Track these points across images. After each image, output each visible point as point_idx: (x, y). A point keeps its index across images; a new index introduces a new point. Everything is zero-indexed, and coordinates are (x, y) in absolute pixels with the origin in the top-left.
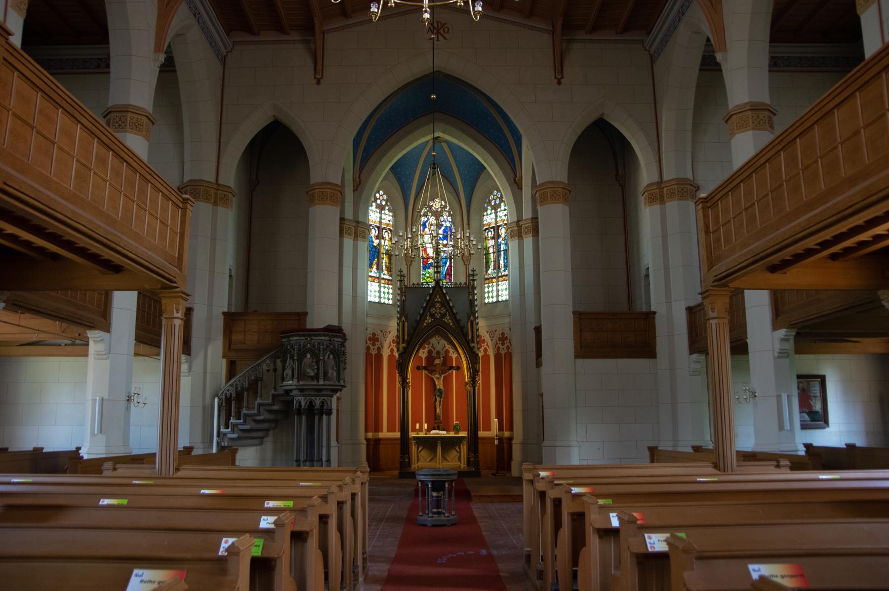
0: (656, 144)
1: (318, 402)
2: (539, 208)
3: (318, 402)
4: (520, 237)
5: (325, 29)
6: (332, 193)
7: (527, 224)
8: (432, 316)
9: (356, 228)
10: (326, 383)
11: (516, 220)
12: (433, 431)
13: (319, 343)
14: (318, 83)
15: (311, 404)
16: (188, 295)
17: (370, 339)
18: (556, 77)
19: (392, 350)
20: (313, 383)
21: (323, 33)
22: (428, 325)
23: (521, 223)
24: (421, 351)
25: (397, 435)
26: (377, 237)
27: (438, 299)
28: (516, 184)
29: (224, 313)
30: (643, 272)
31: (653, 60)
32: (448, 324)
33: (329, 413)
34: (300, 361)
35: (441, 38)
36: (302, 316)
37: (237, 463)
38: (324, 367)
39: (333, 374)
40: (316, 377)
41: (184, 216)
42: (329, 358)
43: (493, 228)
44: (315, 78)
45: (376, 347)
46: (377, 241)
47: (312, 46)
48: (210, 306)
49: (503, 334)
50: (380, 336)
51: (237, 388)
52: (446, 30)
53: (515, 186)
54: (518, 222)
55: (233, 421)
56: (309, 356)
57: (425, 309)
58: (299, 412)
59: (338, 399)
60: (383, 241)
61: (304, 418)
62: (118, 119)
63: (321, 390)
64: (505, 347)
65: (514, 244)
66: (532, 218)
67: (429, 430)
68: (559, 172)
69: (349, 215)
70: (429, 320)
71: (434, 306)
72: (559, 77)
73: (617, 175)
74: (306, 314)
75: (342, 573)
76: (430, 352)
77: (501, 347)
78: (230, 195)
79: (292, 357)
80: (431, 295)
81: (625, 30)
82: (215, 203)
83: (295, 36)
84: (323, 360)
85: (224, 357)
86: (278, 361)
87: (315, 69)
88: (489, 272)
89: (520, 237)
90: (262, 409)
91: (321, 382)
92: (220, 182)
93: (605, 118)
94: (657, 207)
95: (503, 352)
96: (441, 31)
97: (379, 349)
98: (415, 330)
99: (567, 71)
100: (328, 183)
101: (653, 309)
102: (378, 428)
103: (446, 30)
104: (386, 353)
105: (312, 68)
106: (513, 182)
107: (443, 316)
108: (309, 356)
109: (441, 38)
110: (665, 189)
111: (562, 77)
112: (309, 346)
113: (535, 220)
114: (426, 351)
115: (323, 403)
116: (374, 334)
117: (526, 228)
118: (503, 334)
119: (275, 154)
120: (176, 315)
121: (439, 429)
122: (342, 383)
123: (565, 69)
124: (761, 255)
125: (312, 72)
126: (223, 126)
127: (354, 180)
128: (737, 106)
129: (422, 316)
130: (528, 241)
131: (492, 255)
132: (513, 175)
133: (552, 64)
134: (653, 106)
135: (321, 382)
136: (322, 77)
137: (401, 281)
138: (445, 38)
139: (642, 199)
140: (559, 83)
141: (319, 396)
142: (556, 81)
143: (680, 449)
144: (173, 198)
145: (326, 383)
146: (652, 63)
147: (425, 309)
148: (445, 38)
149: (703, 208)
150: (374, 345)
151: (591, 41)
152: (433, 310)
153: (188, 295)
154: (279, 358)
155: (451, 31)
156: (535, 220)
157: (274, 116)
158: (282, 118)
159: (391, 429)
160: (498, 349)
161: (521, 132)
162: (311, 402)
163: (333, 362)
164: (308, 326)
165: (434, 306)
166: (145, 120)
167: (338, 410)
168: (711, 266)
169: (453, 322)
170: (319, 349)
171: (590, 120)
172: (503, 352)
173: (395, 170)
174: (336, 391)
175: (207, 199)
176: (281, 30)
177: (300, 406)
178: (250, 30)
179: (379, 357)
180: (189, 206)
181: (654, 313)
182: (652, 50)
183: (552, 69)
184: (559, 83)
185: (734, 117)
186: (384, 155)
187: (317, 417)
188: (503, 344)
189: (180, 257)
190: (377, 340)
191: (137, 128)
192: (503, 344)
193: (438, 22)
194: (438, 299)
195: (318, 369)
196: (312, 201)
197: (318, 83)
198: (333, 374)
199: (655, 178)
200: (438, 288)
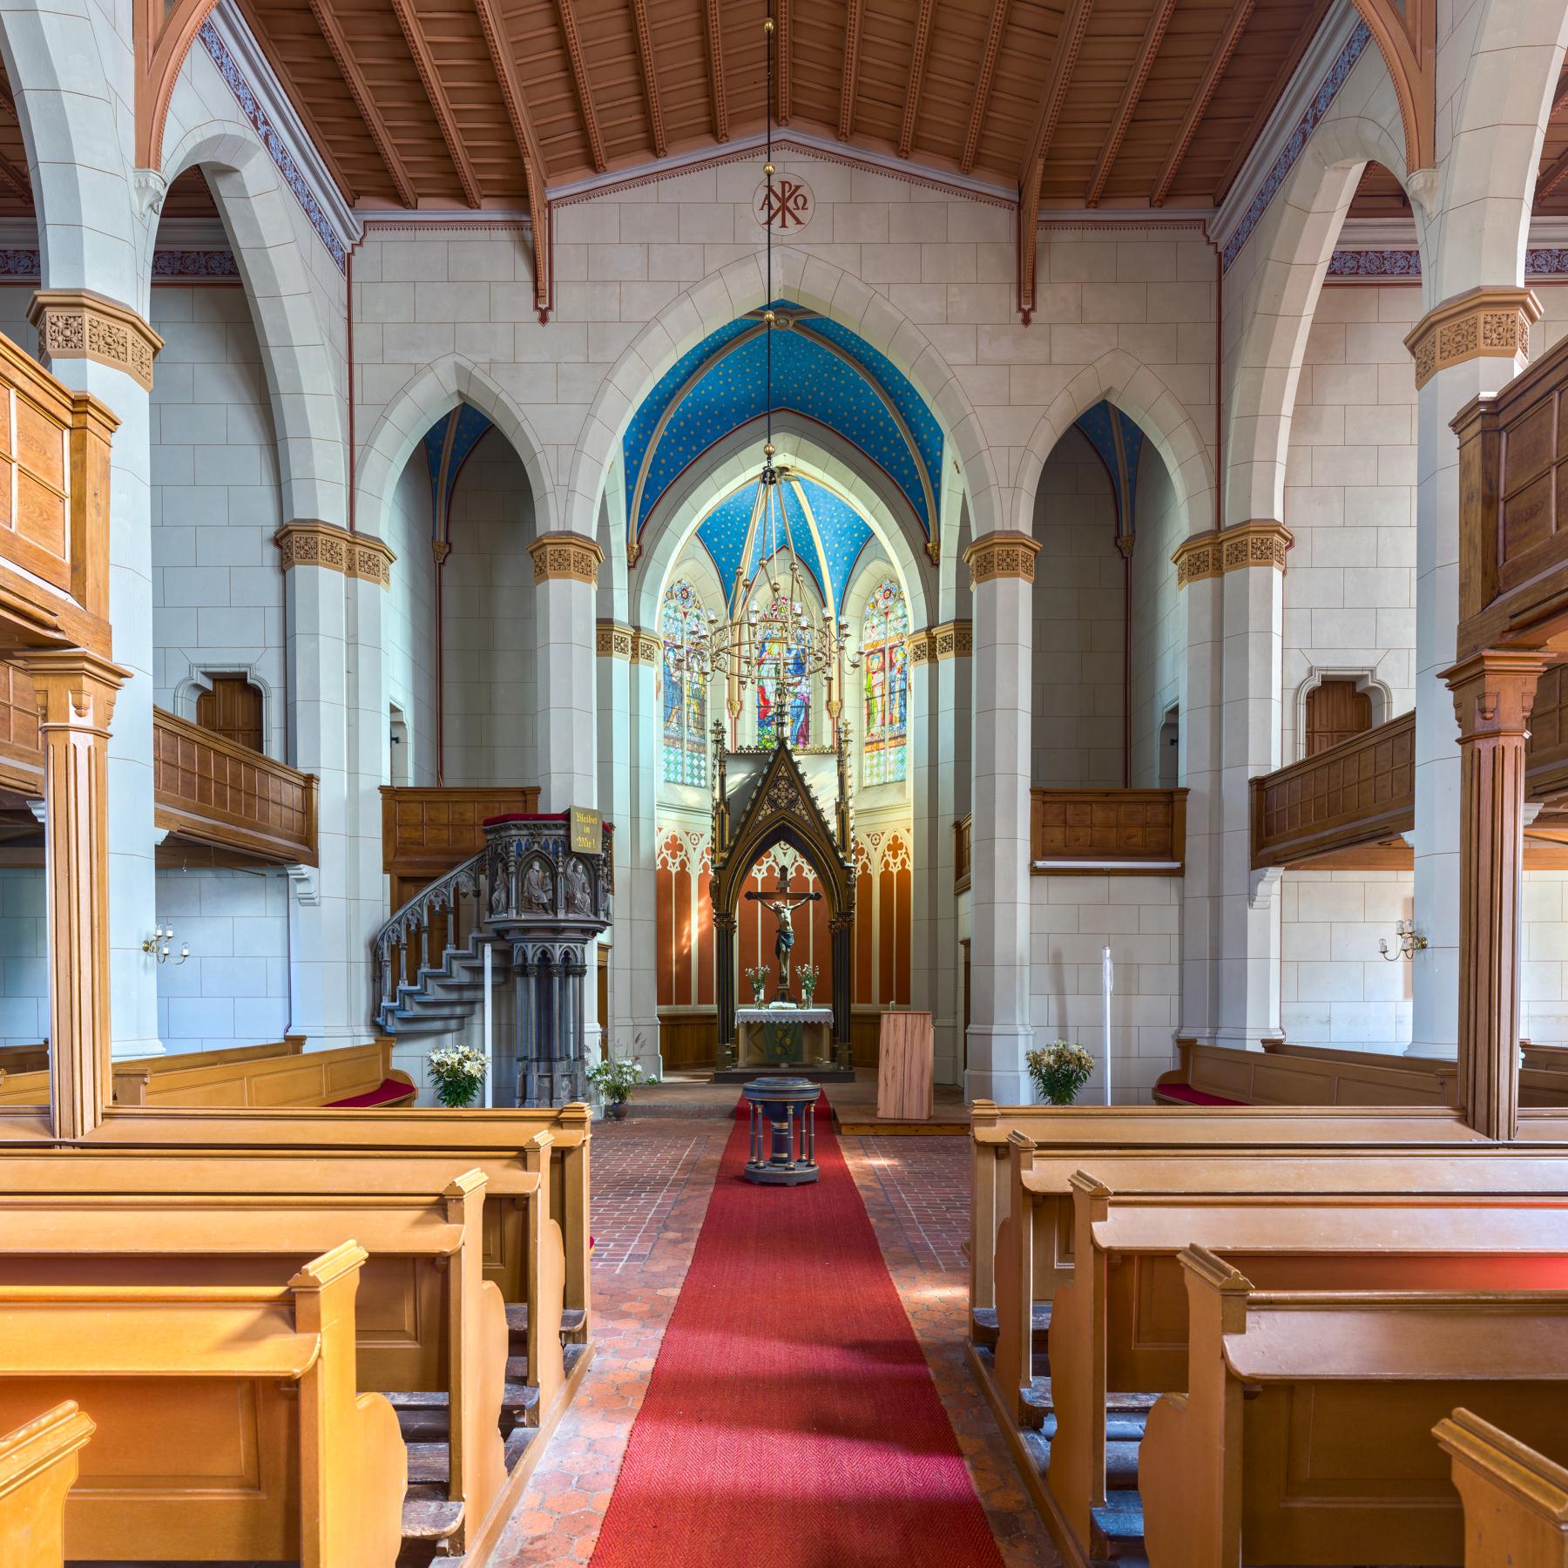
0: (1212, 451)
1: (557, 952)
2: (974, 587)
3: (557, 952)
4: (933, 658)
5: (551, 196)
6: (583, 555)
7: (944, 631)
8: (773, 802)
9: (635, 639)
10: (571, 916)
11: (925, 625)
12: (774, 1004)
13: (555, 842)
14: (543, 319)
15: (545, 957)
16: (122, 675)
17: (667, 846)
18: (1020, 309)
19: (705, 867)
20: (546, 917)
21: (549, 205)
22: (766, 817)
23: (934, 631)
24: (755, 867)
25: (713, 1008)
26: (679, 668)
27: (783, 772)
28: (928, 558)
29: (382, 789)
30: (1160, 719)
31: (1222, 264)
32: (801, 817)
33: (581, 972)
34: (522, 878)
35: (789, 220)
36: (530, 794)
37: (1273, 880)
38: (566, 886)
39: (583, 898)
40: (553, 906)
41: (79, 448)
42: (575, 869)
43: (882, 651)
44: (536, 308)
45: (678, 861)
46: (678, 673)
47: (528, 235)
48: (354, 773)
49: (895, 838)
50: (688, 846)
51: (408, 926)
52: (800, 201)
53: (926, 560)
54: (929, 629)
55: (403, 986)
56: (536, 866)
57: (760, 790)
58: (524, 971)
59: (603, 948)
60: (687, 675)
61: (533, 981)
62: (60, 324)
63: (564, 929)
64: (898, 860)
65: (917, 673)
66: (956, 621)
67: (768, 1000)
68: (1018, 515)
69: (621, 613)
70: (767, 810)
71: (775, 786)
72: (1026, 307)
73: (1117, 537)
74: (537, 791)
75: (960, 829)
76: (770, 869)
77: (891, 861)
78: (382, 557)
79: (506, 869)
80: (771, 766)
81: (1172, 193)
82: (351, 571)
83: (490, 211)
84: (565, 873)
85: (386, 870)
86: (482, 877)
87: (536, 290)
88: (873, 731)
89: (933, 658)
90: (455, 964)
91: (561, 916)
92: (357, 528)
93: (1113, 400)
94: (1206, 584)
95: (895, 871)
96: (791, 204)
97: (683, 864)
98: (744, 825)
99: (1045, 293)
100: (570, 534)
101: (1182, 784)
102: (684, 998)
103: (800, 201)
104: (695, 871)
105: (530, 286)
106: (921, 551)
107: (793, 802)
108: (536, 866)
109: (789, 220)
110: (1225, 545)
111: (1033, 309)
112: (536, 847)
113: (963, 625)
114: (764, 867)
115: (567, 953)
116: (674, 838)
117: (944, 639)
118: (895, 838)
119: (470, 474)
120: (74, 720)
121: (783, 999)
122: (603, 918)
123: (1040, 288)
124: (1525, 616)
125: (531, 295)
126: (356, 408)
127: (629, 548)
128: (1449, 301)
129: (754, 802)
130: (947, 663)
131: (879, 700)
132: (922, 539)
133: (1014, 280)
134: (1214, 368)
135: (561, 916)
136: (550, 308)
137: (717, 742)
138: (799, 222)
139: (1170, 570)
140: (1026, 321)
141: (555, 940)
142: (1020, 315)
143: (1222, 1044)
144: (19, 379)
145: (571, 916)
146: (1221, 270)
147: (760, 790)
148: (799, 222)
149: (1483, 432)
150: (674, 856)
151: (1097, 225)
152: (774, 793)
153: (122, 675)
154: (482, 871)
155: (810, 205)
156: (963, 625)
157: (460, 394)
158: (475, 396)
159: (704, 998)
160: (887, 864)
161: (945, 429)
162: (544, 953)
163: (584, 878)
164: (541, 811)
165: (775, 786)
166: (131, 334)
167: (602, 969)
168: (1492, 591)
169: (809, 814)
170: (556, 854)
171: (1082, 407)
172: (895, 871)
173: (704, 534)
174: (594, 933)
175: (333, 562)
176: (461, 195)
177: (525, 959)
178: (396, 196)
179: (683, 877)
180: (90, 422)
181: (1186, 791)
182: (1223, 242)
183: (1015, 287)
184: (1026, 321)
185: (1438, 330)
186: (683, 497)
187: (556, 980)
188: (895, 856)
189: (78, 567)
190: (681, 848)
191: (112, 351)
192: (895, 856)
193: (783, 183)
194: (783, 772)
195: (555, 890)
196: (541, 574)
197: (543, 319)
198: (583, 898)
199: (1207, 523)
200: (782, 754)
